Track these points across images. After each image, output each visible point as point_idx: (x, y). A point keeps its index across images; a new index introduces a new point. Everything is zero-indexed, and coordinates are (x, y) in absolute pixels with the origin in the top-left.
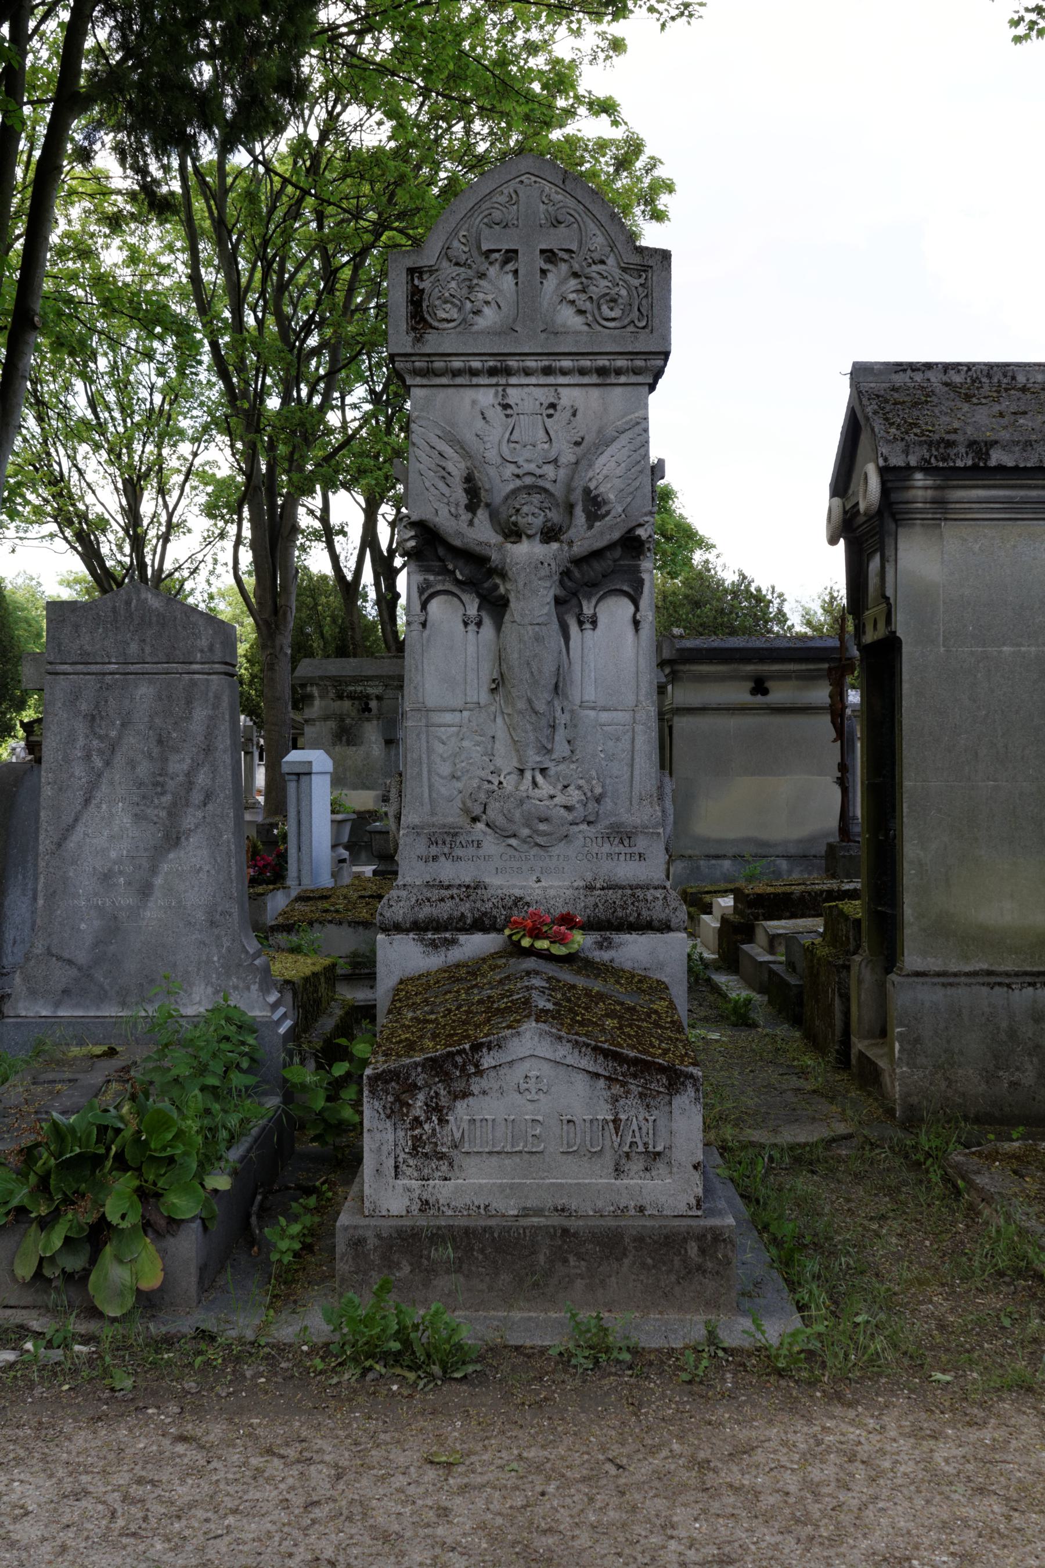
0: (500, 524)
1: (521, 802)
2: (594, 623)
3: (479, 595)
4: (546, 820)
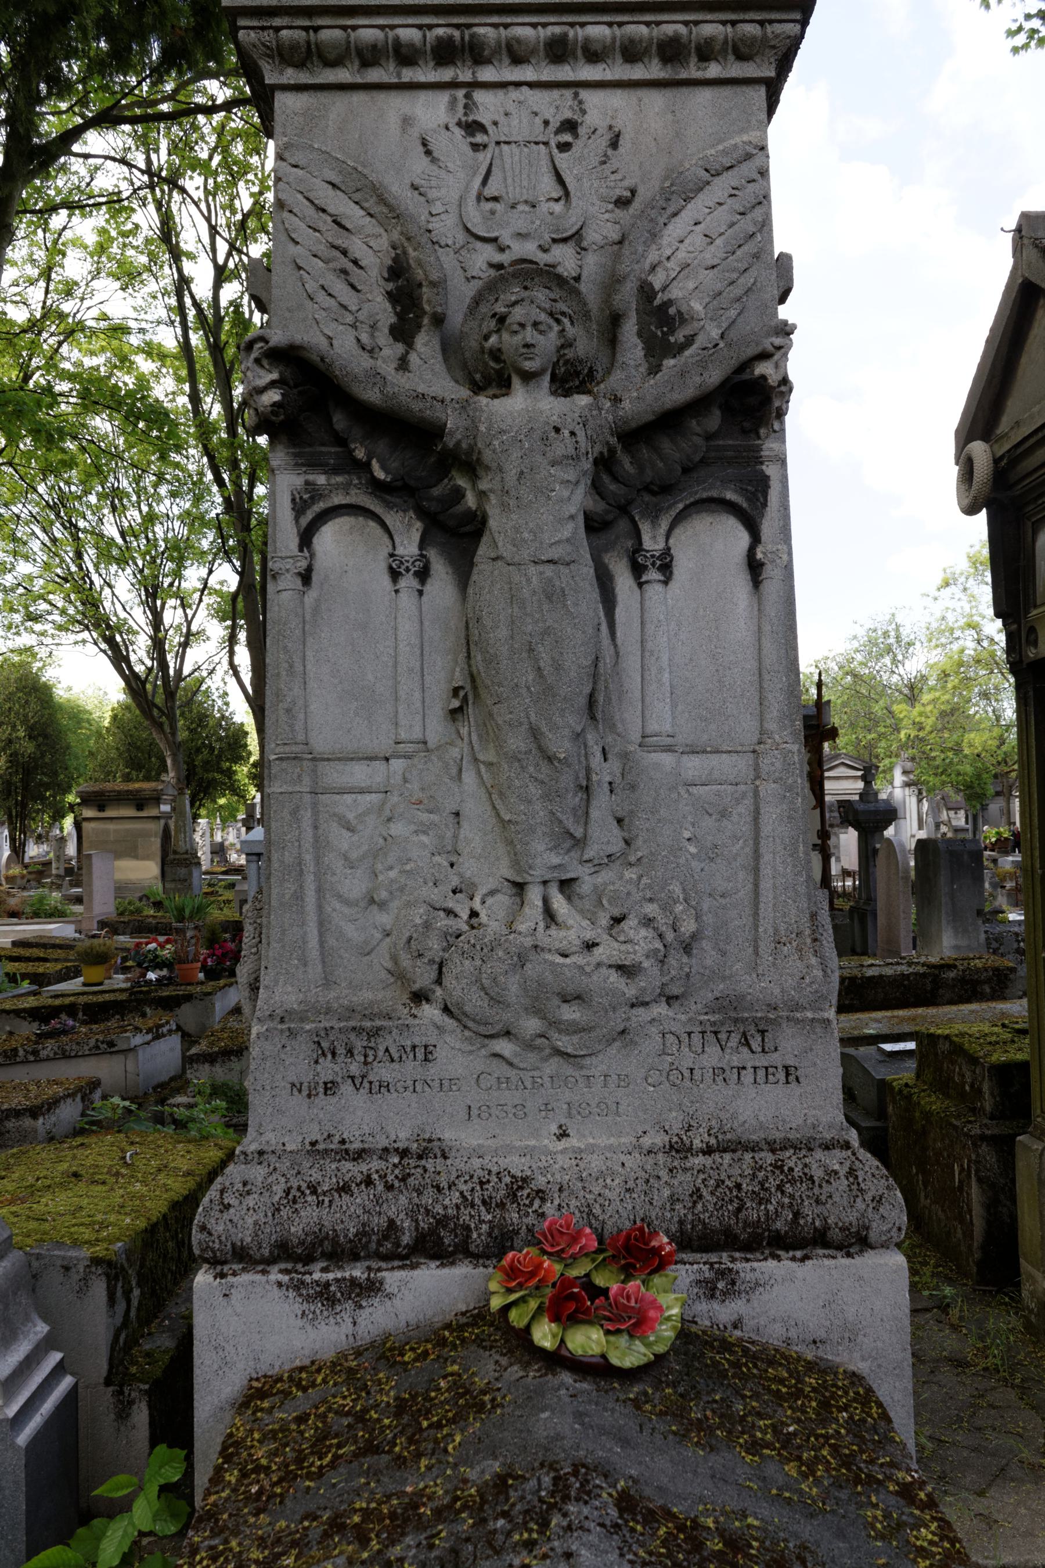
0: (465, 366)
1: (522, 960)
2: (666, 567)
3: (422, 514)
4: (578, 997)
